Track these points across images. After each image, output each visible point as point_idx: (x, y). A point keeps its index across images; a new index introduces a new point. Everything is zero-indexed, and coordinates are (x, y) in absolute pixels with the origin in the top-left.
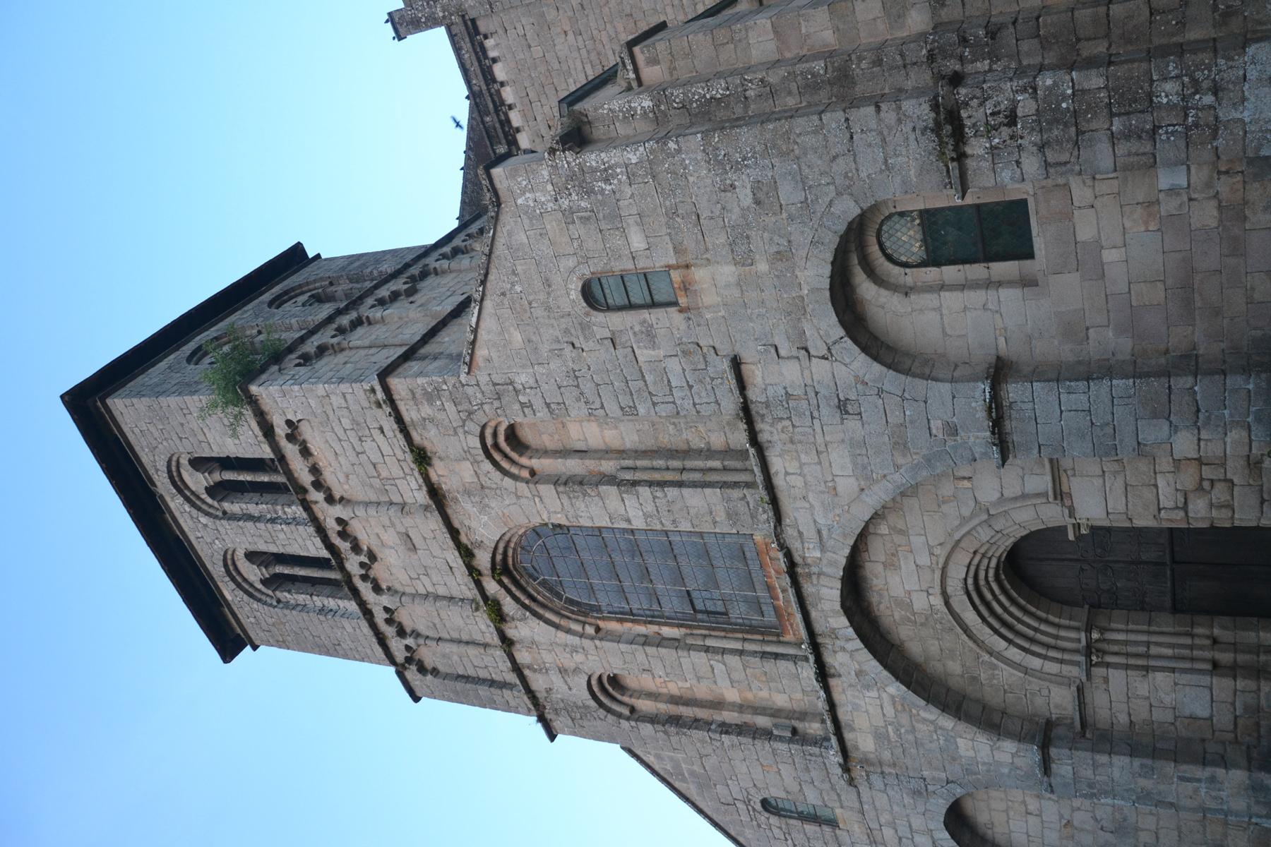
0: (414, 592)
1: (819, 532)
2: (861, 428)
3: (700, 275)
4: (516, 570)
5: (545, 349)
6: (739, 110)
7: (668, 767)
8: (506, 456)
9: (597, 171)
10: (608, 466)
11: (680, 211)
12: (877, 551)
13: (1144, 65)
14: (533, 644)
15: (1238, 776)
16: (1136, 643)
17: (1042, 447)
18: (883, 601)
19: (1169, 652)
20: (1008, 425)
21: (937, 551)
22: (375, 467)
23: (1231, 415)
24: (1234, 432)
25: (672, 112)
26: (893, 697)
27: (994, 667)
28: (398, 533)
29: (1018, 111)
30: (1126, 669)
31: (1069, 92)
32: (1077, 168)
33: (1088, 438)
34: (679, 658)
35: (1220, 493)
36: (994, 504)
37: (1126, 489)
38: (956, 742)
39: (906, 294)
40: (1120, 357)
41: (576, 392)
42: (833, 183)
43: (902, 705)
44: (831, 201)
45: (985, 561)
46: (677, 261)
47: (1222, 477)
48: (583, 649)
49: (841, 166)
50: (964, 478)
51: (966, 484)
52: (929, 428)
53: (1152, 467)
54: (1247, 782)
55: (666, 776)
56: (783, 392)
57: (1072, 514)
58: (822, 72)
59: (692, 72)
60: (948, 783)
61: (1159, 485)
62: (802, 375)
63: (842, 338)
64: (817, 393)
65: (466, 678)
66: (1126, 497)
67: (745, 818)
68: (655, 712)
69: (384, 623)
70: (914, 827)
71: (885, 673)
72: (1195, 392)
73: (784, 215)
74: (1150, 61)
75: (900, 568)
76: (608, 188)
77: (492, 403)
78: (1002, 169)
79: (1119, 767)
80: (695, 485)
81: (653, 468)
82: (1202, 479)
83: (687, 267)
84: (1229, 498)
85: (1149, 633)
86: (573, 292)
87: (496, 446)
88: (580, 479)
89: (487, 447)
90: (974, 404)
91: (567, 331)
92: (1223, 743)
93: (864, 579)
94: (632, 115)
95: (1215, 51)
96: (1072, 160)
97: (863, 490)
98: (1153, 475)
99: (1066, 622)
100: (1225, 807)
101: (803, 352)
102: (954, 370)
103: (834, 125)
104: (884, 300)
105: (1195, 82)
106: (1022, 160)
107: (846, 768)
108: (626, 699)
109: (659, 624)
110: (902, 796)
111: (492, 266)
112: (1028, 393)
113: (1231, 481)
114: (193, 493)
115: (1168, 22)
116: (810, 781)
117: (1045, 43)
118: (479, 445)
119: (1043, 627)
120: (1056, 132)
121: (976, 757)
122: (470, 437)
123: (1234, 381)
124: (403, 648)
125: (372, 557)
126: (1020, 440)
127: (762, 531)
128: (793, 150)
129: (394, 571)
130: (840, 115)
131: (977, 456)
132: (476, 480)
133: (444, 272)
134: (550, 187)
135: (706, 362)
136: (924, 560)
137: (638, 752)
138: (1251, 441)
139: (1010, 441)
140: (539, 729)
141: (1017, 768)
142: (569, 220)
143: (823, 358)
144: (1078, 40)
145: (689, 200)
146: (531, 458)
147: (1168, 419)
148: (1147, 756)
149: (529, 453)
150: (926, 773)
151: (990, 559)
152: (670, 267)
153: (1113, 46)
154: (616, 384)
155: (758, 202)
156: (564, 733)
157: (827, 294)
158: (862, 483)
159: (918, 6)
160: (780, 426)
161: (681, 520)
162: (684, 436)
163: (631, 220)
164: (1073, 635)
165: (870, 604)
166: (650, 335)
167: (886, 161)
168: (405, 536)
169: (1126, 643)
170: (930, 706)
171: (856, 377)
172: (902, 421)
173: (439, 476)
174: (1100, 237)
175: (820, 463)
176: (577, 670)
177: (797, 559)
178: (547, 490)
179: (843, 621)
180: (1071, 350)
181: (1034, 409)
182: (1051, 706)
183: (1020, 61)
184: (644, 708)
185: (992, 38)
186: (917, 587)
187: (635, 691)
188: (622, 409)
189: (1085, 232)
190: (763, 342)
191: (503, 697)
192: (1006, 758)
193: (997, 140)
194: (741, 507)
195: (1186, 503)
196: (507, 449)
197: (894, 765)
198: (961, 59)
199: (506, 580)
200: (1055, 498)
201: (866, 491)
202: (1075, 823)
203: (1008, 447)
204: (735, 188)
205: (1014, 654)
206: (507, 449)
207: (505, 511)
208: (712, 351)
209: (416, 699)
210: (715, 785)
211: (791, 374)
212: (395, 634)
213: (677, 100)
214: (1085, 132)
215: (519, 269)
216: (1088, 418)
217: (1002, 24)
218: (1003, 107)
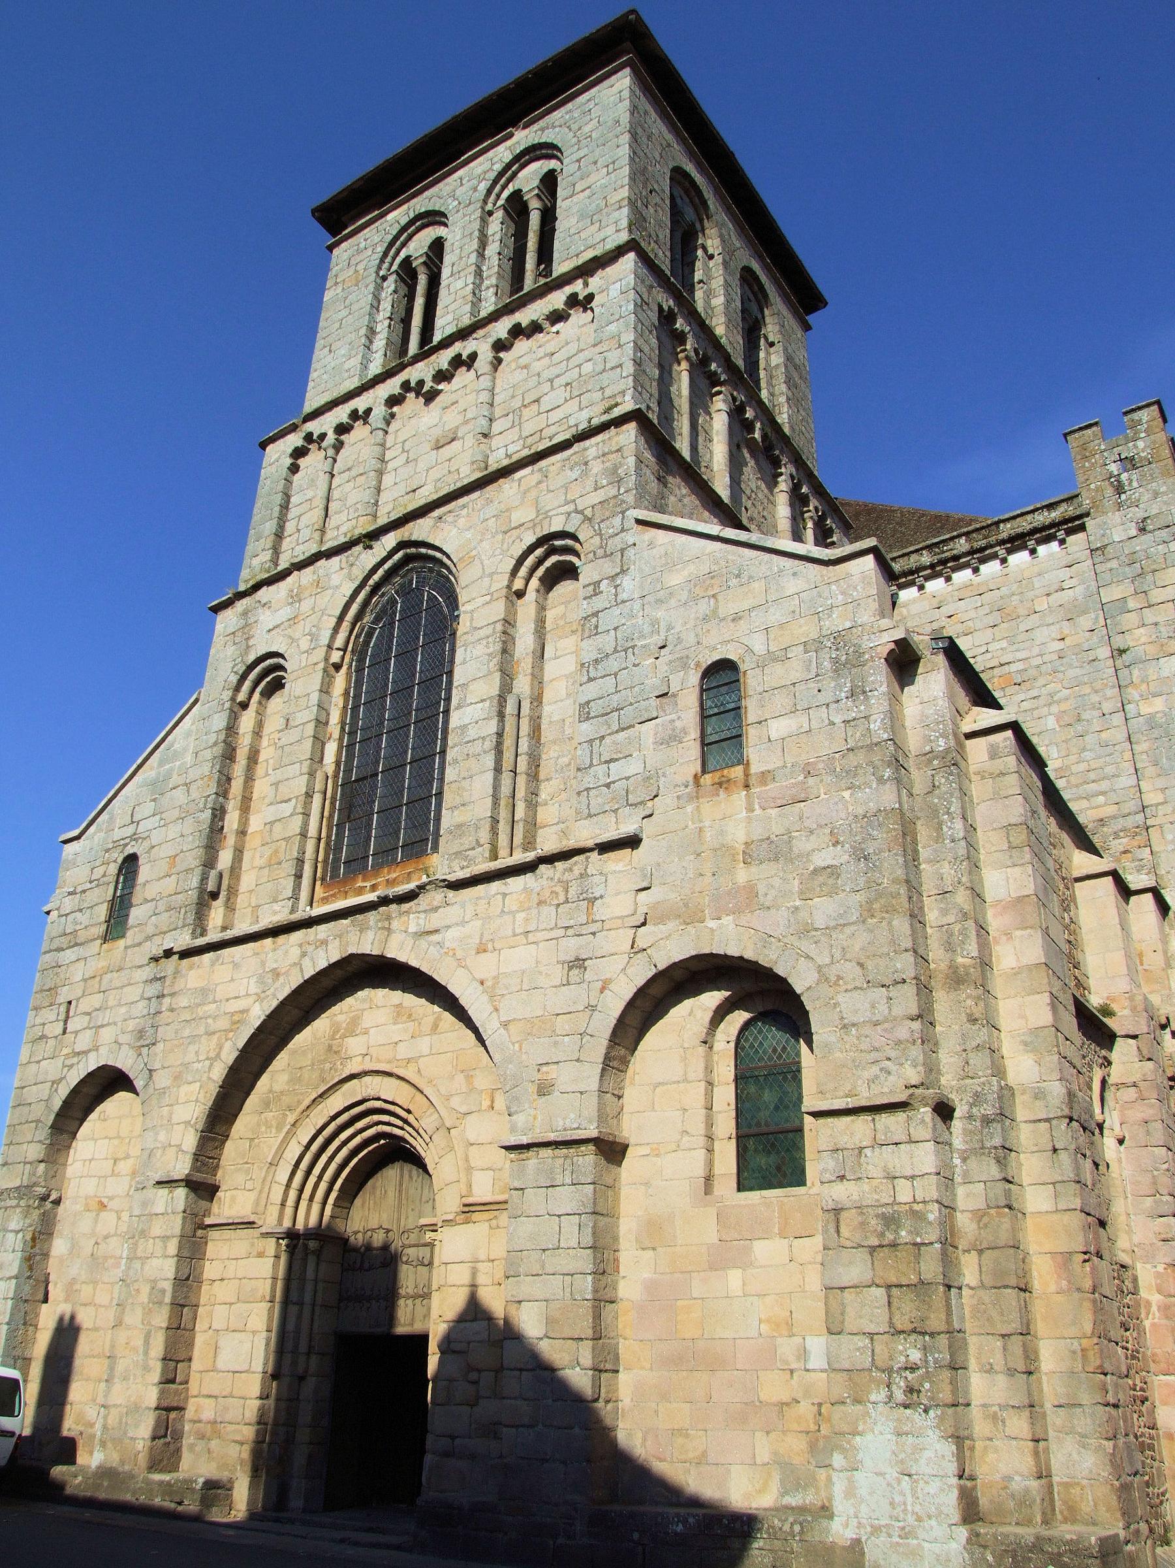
1: (437, 931)
3: (739, 797)
10: (522, 685)
16: (302, 1289)
28: (457, 427)
31: (918, 1240)
34: (301, 762)
49: (851, 971)
51: (486, 1103)
56: (597, 895)
61: (475, 1324)
64: (594, 934)
67: (118, 834)
71: (275, 1003)
75: (395, 1024)
77: (601, 547)
82: (479, 1371)
91: (679, 640)
97: (482, 983)
108: (256, 696)
114: (515, 174)
131: (514, 1117)
134: (848, 625)
135: (636, 805)
148: (174, 1297)
150: (160, 1046)
154: (615, 697)
160: (559, 889)
166: (672, 739)
182: (234, 1192)
188: (588, 703)
194: (468, 841)
195: (454, 1352)
200: (465, 1205)
201: (481, 988)
202: (103, 1214)
204: (834, 845)
210: (154, 800)
215: (756, 585)
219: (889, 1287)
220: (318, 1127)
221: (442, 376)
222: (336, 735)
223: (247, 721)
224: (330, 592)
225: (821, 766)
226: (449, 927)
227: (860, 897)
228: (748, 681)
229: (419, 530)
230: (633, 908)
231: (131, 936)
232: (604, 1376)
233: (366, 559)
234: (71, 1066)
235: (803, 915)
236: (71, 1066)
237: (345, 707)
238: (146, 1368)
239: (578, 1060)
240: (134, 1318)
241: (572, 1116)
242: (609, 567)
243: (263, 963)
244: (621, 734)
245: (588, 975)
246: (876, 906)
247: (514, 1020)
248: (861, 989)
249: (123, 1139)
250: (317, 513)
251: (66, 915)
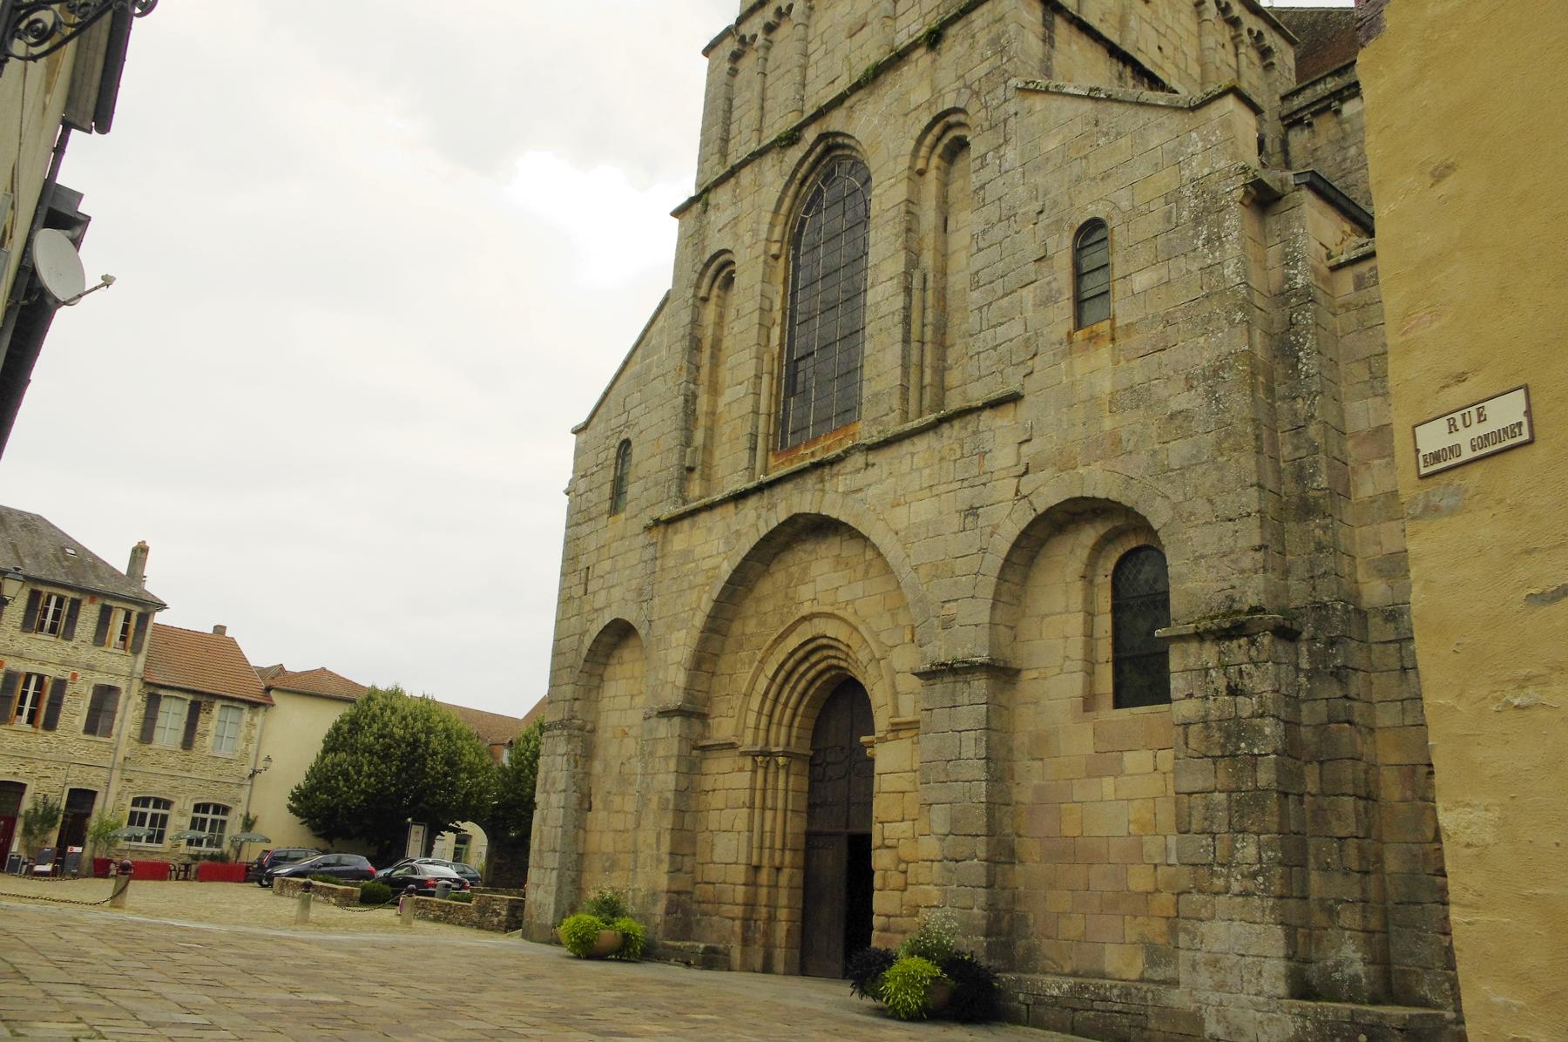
0: (809, 39)
1: (860, 490)
3: (1104, 352)
4: (831, 160)
5: (1038, 179)
6: (1281, 390)
7: (654, 342)
8: (939, 139)
9: (1219, 228)
10: (928, 259)
11: (1169, 328)
12: (850, 550)
13: (1275, 827)
14: (759, 186)
15: (663, 882)
16: (775, 798)
19: (768, 827)
20: (949, 679)
21: (850, 609)
23: (952, 891)
25: (1288, 312)
27: (751, 664)
28: (867, 13)
29: (1242, 697)
30: (751, 788)
31: (1256, 751)
32: (1181, 756)
34: (750, 348)
36: (890, 665)
38: (682, 629)
39: (1083, 577)
40: (1015, 790)
41: (994, 219)
42: (1186, 500)
43: (712, 577)
44: (1168, 498)
45: (843, 657)
46: (1120, 327)
47: (909, 881)
49: (1202, 508)
51: (908, 637)
52: (949, 601)
55: (646, 339)
56: (987, 449)
57: (883, 740)
58: (1315, 484)
59: (1342, 331)
62: (1002, 469)
63: (1035, 510)
64: (984, 484)
65: (729, 110)
67: (614, 423)
68: (704, 324)
69: (776, 6)
70: (612, 590)
71: (739, 559)
72: (972, 859)
73: (1157, 446)
74: (1280, 834)
75: (835, 572)
76: (1200, 243)
77: (987, 119)
78: (1186, 679)
79: (666, 780)
80: (905, 357)
81: (924, 309)
82: (908, 863)
83: (1113, 339)
84: (891, 887)
85: (785, 810)
86: (1094, 208)
87: (949, 127)
88: (914, 227)
89: (945, 117)
90: (969, 645)
91: (1055, 203)
92: (692, 872)
93: (825, 536)
94: (1287, 264)
95: (1281, 897)
96: (1189, 751)
97: (897, 534)
98: (912, 817)
99: (794, 731)
100: (638, 870)
101: (1023, 470)
102: (1006, 626)
103: (1244, 499)
104: (1078, 554)
105: (1254, 876)
106: (1193, 700)
107: (657, 522)
108: (715, 291)
109: (783, 324)
111: (1128, 106)
112: (977, 700)
113: (904, 890)
115: (1330, 855)
117: (1320, 728)
118: (946, 107)
119: (789, 712)
120: (1217, 735)
122: (954, 95)
123: (982, 896)
124: (753, 33)
127: (866, 432)
128: (1222, 455)
129: (830, 12)
130: (1254, 507)
131: (924, 648)
132: (912, 107)
133: (1199, 14)
134: (1206, 171)
135: (1018, 365)
136: (843, 596)
137: (666, 309)
140: (683, 200)
141: (663, 687)
142: (1169, 198)
143: (1018, 491)
144: (1321, 763)
145: (1180, 339)
146: (938, 168)
147: (950, 833)
148: (676, 805)
149: (943, 164)
150: (656, 601)
151: (846, 661)
152: (1113, 319)
153: (1311, 798)
154: (1001, 265)
155: (1172, 416)
156: (681, 226)
157: (1078, 494)
158: (903, 533)
159: (1390, 592)
160: (956, 446)
162: (958, 341)
163: (1164, 271)
164: (783, 740)
165: (804, 541)
166: (1048, 300)
167: (1202, 557)
168: (862, 22)
169: (775, 789)
170: (711, 604)
171: (998, 526)
172: (957, 573)
173: (917, 61)
174: (1125, 775)
176: (737, 237)
177: (836, 468)
178: (901, 191)
180: (1023, 743)
183: (1304, 701)
184: (707, 311)
185: (1332, 673)
187: (724, 300)
188: (977, 273)
189: (1130, 759)
190: (1034, 426)
193: (1214, 674)
194: (883, 408)
195: (888, 847)
196: (946, 140)
197: (663, 570)
198: (1313, 639)
199: (819, 149)
200: (893, 724)
202: (626, 740)
204: (1188, 390)
205: (762, 684)
206: (946, 140)
208: (1028, 371)
209: (706, 52)
210: (640, 391)
211: (1004, 457)
212: (766, 20)
213: (1300, 317)
214: (1215, 764)
215: (1122, 141)
217: (1346, 684)
218: (1247, 681)
220: (780, 662)
222: (779, 320)
223: (710, 313)
224: (766, 188)
225: (1179, 314)
226: (870, 485)
227: (1211, 438)
228: (1115, 238)
229: (835, 122)
230: (1015, 459)
231: (630, 508)
232: (999, 868)
233: (795, 154)
234: (592, 620)
235: (1161, 456)
236: (592, 620)
237: (785, 294)
238: (659, 861)
240: (649, 822)
241: (969, 645)
242: (991, 138)
243: (728, 526)
244: (1006, 299)
245: (981, 522)
246: (1225, 445)
247: (922, 564)
248: (1211, 524)
249: (636, 678)
250: (755, 113)
251: (581, 495)
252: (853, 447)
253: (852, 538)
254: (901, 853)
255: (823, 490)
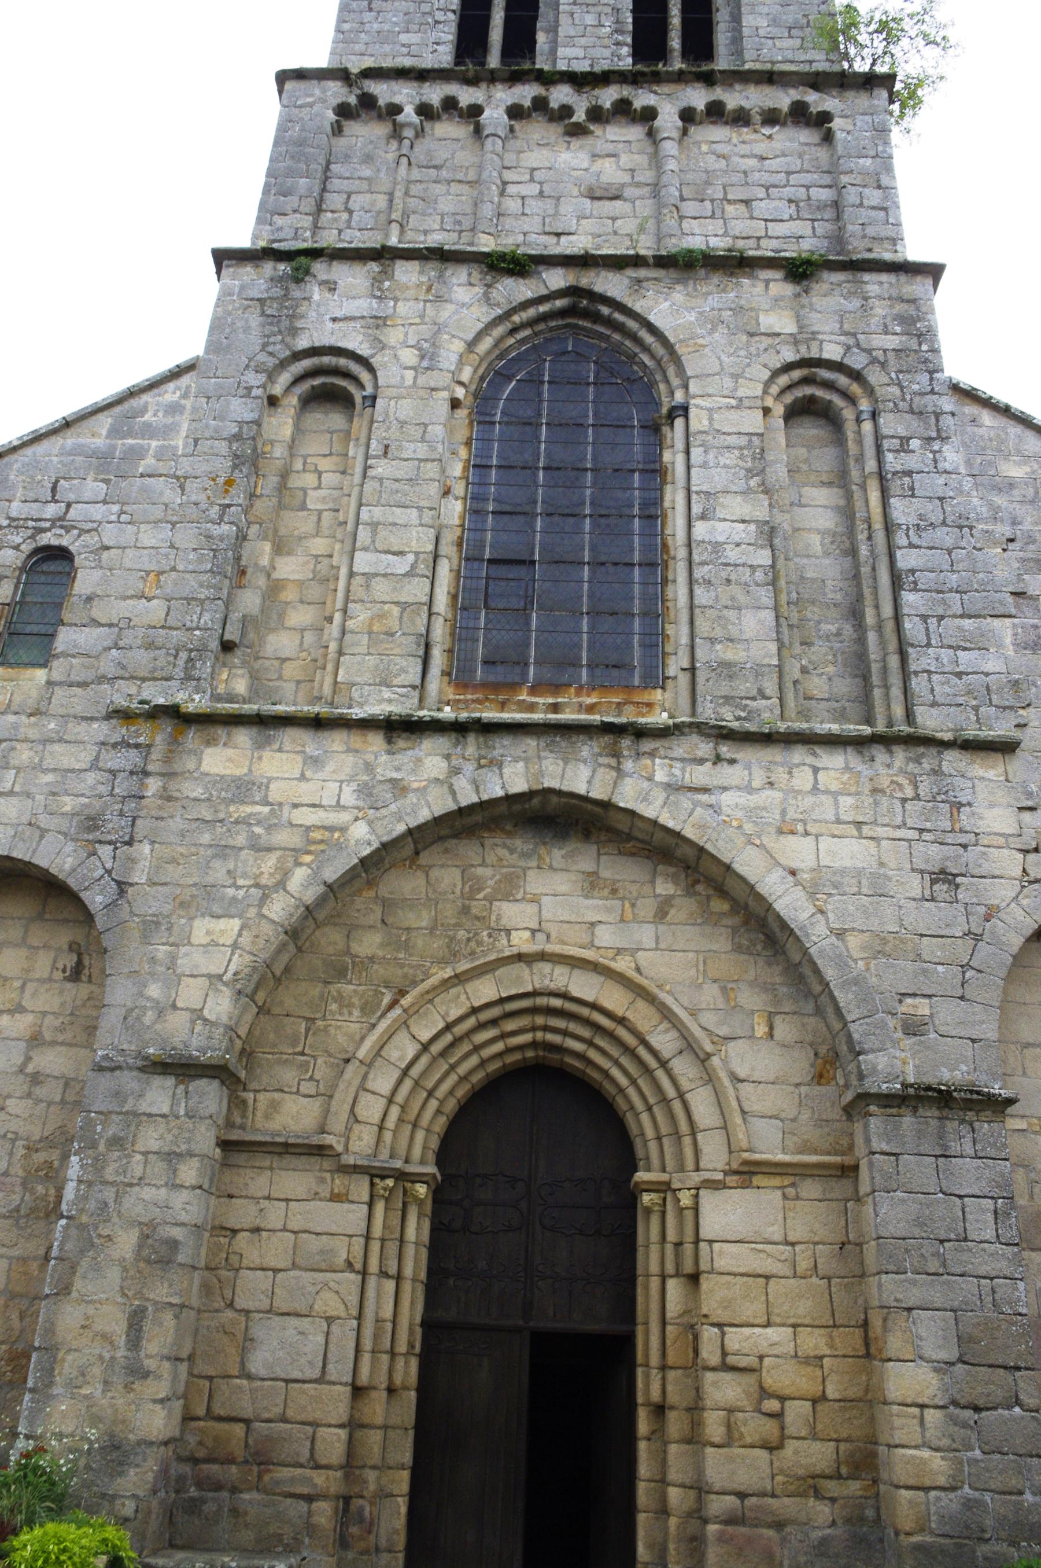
1: (705, 790)
2: (908, 895)
4: (566, 326)
17: (893, 1158)
18: (515, 856)
22: (742, 201)
24: (943, 1463)
26: (343, 830)
33: (917, 1232)
35: (754, 1427)
37: (760, 1276)
47: (791, 1430)
48: (427, 369)
50: (771, 1028)
53: (807, 1321)
54: (131, 1436)
60: (119, 883)
61: (769, 1330)
64: (965, 846)
66: (742, 1275)
75: (587, 897)
82: (782, 1399)
84: (748, 1440)
98: (792, 1321)
100: (56, 1390)
110: (82, 795)
116: (121, 643)
121: (189, 943)
125: (577, 131)
126: (905, 1127)
138: (926, 1489)
139: (902, 1111)
161: (713, 594)
175: (838, 821)
177: (647, 745)
179: (519, 785)
181: (962, 1156)
182: (277, 1095)
186: (545, 915)
191: (295, 211)
192: (190, 994)
199: (559, 303)
200: (746, 1163)
201: (791, 878)
203: (890, 1107)
207: (707, 350)
210: (106, 481)
212: (424, 99)
216: (953, 1236)
219: (794, 1326)
221: (596, 114)
226: (725, 789)
239: (962, 998)
241: (964, 1068)
247: (853, 929)
252: (691, 725)
253: (620, 853)
254: (768, 1381)
255: (618, 769)
